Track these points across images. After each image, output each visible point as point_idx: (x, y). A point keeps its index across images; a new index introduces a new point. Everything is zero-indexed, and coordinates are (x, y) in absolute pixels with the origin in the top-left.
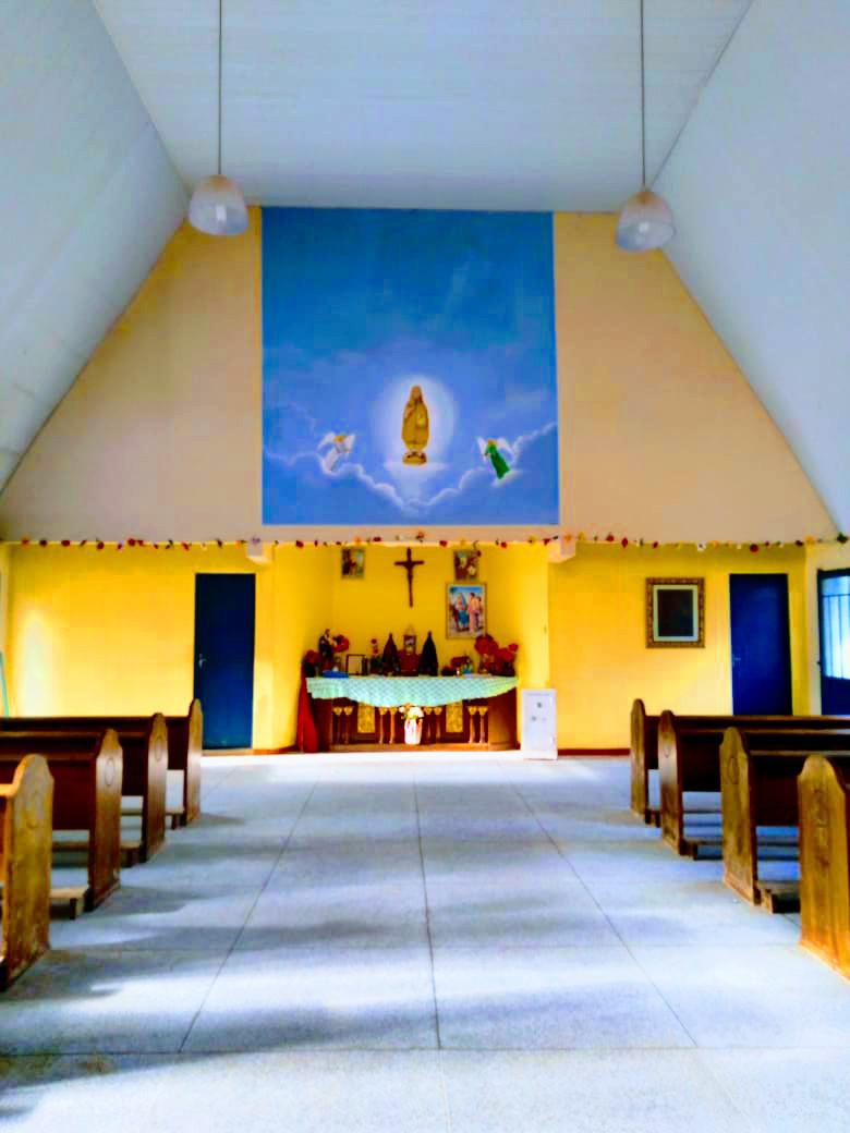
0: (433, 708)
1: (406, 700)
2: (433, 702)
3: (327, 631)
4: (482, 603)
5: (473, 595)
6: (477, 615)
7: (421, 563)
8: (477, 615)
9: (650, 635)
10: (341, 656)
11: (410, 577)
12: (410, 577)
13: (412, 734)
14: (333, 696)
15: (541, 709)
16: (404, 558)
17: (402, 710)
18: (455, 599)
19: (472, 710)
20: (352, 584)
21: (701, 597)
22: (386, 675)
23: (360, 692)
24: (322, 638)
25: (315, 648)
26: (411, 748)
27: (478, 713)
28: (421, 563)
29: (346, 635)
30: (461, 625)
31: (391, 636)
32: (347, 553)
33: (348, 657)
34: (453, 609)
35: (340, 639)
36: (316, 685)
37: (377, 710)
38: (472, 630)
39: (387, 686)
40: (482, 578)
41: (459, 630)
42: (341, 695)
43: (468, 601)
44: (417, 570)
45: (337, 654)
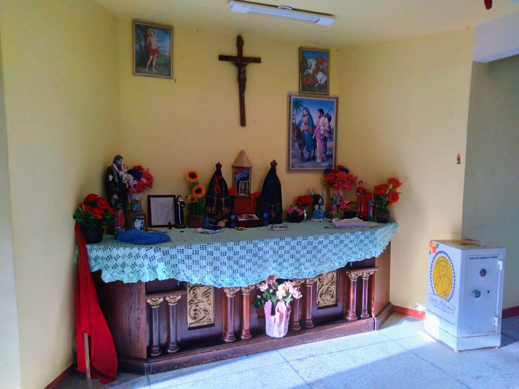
0: (306, 280)
1: (272, 270)
2: (308, 272)
3: (118, 158)
4: (332, 123)
5: (321, 111)
6: (325, 140)
7: (257, 60)
8: (325, 140)
9: (133, 73)
10: (140, 197)
13: (276, 327)
14: (147, 278)
15: (489, 290)
16: (232, 51)
17: (264, 288)
18: (299, 118)
19: (353, 276)
20: (152, 84)
22: (215, 227)
24: (109, 171)
25: (97, 190)
26: (276, 345)
27: (360, 279)
28: (257, 60)
29: (145, 165)
31: (219, 166)
33: (149, 197)
35: (137, 172)
36: (109, 258)
37: (219, 293)
38: (319, 160)
39: (242, 253)
40: (333, 91)
41: (304, 160)
42: (162, 276)
43: (315, 122)
44: (252, 70)
45: (136, 197)
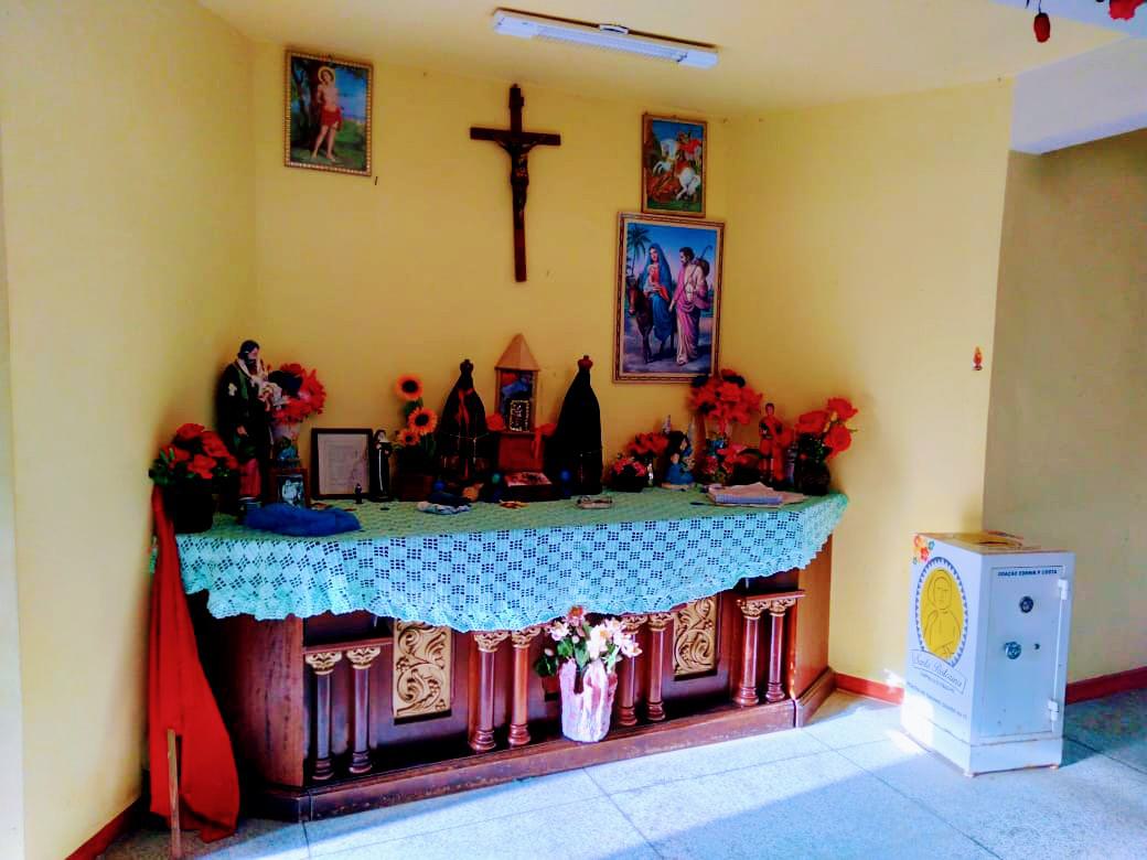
4: (711, 280)
5: (688, 252)
6: (695, 314)
7: (553, 140)
11: (519, 186)
12: (519, 186)
16: (500, 119)
18: (641, 265)
20: (321, 186)
21: (722, 234)
22: (457, 501)
23: (413, 587)
24: (228, 374)
25: (201, 414)
26: (587, 757)
28: (553, 140)
30: (655, 344)
31: (467, 367)
32: (305, 69)
33: (315, 433)
34: (632, 289)
35: (289, 377)
36: (226, 564)
40: (714, 208)
42: (340, 606)
44: (539, 158)
